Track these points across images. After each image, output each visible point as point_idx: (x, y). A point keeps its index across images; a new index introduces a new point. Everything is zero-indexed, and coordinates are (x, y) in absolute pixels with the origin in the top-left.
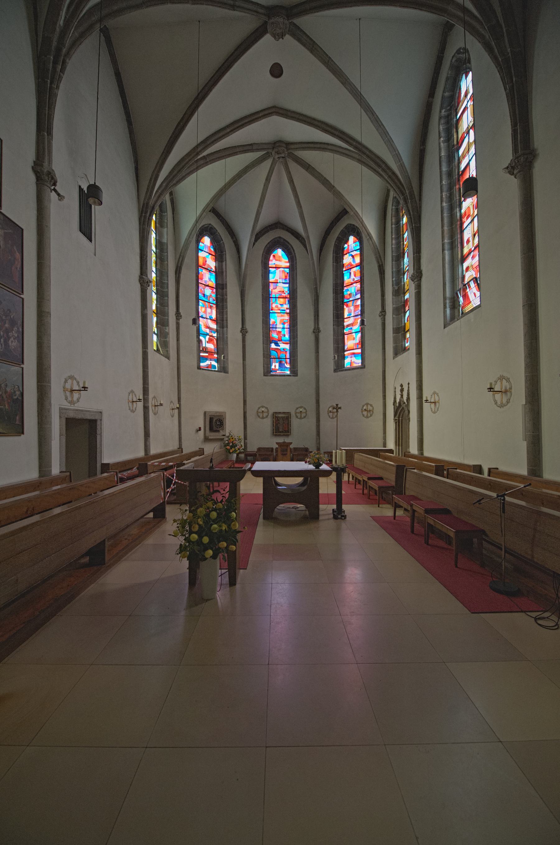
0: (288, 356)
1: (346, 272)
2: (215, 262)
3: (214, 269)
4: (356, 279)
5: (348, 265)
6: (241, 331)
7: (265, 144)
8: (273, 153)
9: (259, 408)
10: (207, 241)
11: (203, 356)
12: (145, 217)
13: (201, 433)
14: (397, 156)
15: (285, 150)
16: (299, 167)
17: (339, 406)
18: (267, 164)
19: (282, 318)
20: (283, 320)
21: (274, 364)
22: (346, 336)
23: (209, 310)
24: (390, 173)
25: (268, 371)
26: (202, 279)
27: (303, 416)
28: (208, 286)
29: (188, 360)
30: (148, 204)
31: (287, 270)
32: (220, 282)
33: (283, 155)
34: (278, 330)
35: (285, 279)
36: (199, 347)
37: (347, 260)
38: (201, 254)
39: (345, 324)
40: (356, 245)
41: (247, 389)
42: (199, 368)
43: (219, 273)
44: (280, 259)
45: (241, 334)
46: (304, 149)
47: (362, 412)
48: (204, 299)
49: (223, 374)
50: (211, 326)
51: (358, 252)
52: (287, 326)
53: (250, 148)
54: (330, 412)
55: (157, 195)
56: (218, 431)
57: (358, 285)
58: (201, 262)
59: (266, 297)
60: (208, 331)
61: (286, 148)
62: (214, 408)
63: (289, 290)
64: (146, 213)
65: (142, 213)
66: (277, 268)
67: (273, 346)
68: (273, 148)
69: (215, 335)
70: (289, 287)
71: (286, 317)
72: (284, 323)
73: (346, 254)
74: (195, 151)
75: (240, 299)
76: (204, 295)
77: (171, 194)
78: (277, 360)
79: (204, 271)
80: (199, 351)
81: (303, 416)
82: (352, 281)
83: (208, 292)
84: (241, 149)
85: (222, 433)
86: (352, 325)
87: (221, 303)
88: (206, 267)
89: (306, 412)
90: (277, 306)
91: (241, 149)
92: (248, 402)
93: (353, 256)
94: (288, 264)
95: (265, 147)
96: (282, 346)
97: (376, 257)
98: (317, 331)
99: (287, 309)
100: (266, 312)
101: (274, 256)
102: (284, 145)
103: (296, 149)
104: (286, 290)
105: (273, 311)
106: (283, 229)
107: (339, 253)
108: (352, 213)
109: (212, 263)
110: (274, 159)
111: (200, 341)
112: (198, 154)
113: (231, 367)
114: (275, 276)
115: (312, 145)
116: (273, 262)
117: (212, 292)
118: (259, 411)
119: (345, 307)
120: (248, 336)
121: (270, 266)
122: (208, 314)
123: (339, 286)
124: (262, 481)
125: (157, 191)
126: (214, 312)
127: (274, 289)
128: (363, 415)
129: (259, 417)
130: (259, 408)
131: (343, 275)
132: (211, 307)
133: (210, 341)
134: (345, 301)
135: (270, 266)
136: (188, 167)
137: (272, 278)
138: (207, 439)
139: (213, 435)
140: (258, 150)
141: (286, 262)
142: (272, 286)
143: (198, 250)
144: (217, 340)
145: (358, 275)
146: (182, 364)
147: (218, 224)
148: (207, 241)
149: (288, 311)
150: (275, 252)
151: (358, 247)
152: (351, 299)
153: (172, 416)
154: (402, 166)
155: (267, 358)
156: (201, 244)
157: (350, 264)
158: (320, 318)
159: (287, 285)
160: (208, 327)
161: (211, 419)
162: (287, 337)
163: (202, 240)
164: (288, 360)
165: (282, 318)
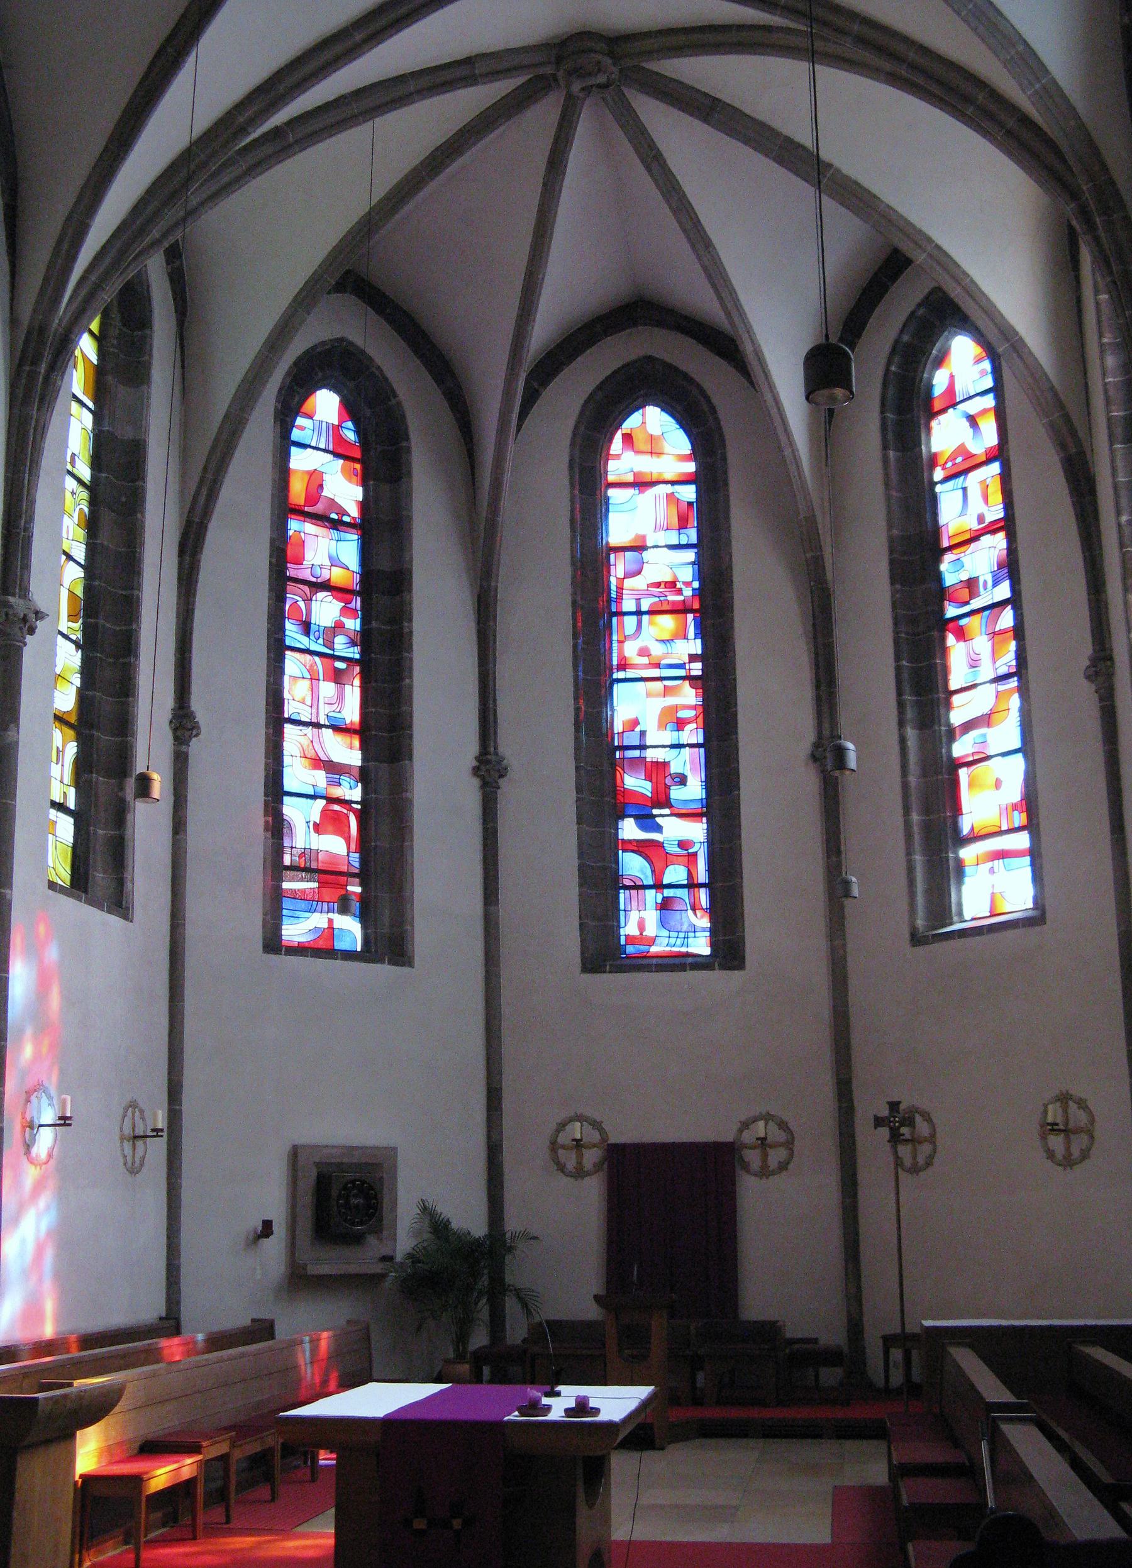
0: (702, 876)
1: (950, 485)
2: (364, 483)
3: (354, 512)
4: (989, 518)
5: (952, 458)
6: (476, 771)
7: (525, 50)
8: (560, 75)
9: (562, 1126)
10: (326, 404)
11: (295, 895)
12: (32, 376)
13: (275, 1247)
14: (1025, 60)
15: (608, 61)
16: (675, 114)
17: (885, 1112)
18: (542, 116)
19: (671, 701)
20: (676, 708)
21: (634, 916)
22: (963, 773)
23: (328, 689)
24: (1011, 123)
25: (604, 951)
26: (299, 561)
27: (773, 1163)
28: (325, 586)
29: (224, 914)
30: (42, 330)
31: (688, 493)
32: (384, 564)
33: (601, 79)
34: (651, 755)
35: (683, 524)
36: (277, 850)
37: (946, 435)
38: (300, 461)
39: (957, 717)
40: (983, 373)
41: (505, 1032)
42: (273, 943)
43: (381, 529)
44: (654, 447)
45: (476, 782)
46: (678, 51)
47: (1043, 1137)
48: (303, 641)
49: (383, 971)
50: (336, 759)
51: (989, 401)
52: (692, 734)
53: (464, 71)
54: (1053, 1128)
55: (83, 293)
56: (357, 1239)
57: (999, 541)
58: (298, 490)
59: (593, 611)
60: (320, 778)
61: (611, 54)
62: (343, 1127)
63: (701, 576)
64: (35, 362)
65: (20, 365)
66: (641, 484)
67: (629, 829)
68: (559, 60)
69: (354, 793)
70: (698, 563)
71: (689, 696)
72: (680, 724)
73: (943, 411)
74: (229, 125)
75: (472, 626)
76: (306, 627)
77: (174, 254)
78: (651, 894)
79: (310, 528)
80: (276, 869)
81: (773, 1163)
82: (975, 526)
83: (326, 610)
84: (424, 82)
85: (374, 1247)
86: (985, 720)
87: (382, 660)
88: (319, 508)
89: (789, 1144)
90: (644, 652)
91: (424, 82)
92: (506, 1105)
93: (972, 420)
94: (691, 467)
95: (527, 59)
96: (675, 830)
97: (1052, 426)
98: (827, 756)
99: (693, 658)
100: (594, 676)
101: (628, 439)
102: (602, 46)
103: (650, 54)
104: (686, 574)
105: (630, 674)
106: (660, 324)
107: (911, 406)
108: (920, 258)
109: (346, 492)
110: (569, 97)
111: (277, 826)
112: (243, 130)
113: (424, 934)
114: (630, 517)
115: (710, 37)
116: (621, 463)
117: (345, 611)
118: (563, 1139)
119: (951, 639)
120: (509, 793)
121: (611, 478)
122: (323, 704)
123: (918, 548)
124: (818, 1541)
125: (83, 278)
126: (353, 694)
127: (629, 575)
128: (1050, 1154)
129: (561, 1168)
130: (562, 1126)
131: (934, 499)
132: (337, 677)
133: (330, 822)
134: (951, 611)
135: (611, 478)
136: (214, 175)
137: (619, 528)
138: (300, 1281)
139: (328, 1262)
140: (506, 72)
141: (684, 458)
142: (619, 566)
143: (285, 444)
144: (363, 817)
145: (996, 497)
146: (192, 932)
147: (381, 337)
148: (326, 404)
149: (697, 669)
150: (632, 422)
151: (988, 382)
152: (976, 604)
153: (134, 1170)
154: (1051, 93)
155: (601, 886)
156: (300, 421)
157: (962, 450)
158: (844, 694)
159: (690, 555)
160: (318, 763)
161: (323, 1183)
162: (693, 790)
163: (307, 407)
164: (703, 896)
165: (671, 701)
